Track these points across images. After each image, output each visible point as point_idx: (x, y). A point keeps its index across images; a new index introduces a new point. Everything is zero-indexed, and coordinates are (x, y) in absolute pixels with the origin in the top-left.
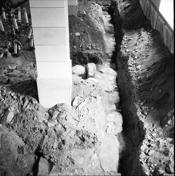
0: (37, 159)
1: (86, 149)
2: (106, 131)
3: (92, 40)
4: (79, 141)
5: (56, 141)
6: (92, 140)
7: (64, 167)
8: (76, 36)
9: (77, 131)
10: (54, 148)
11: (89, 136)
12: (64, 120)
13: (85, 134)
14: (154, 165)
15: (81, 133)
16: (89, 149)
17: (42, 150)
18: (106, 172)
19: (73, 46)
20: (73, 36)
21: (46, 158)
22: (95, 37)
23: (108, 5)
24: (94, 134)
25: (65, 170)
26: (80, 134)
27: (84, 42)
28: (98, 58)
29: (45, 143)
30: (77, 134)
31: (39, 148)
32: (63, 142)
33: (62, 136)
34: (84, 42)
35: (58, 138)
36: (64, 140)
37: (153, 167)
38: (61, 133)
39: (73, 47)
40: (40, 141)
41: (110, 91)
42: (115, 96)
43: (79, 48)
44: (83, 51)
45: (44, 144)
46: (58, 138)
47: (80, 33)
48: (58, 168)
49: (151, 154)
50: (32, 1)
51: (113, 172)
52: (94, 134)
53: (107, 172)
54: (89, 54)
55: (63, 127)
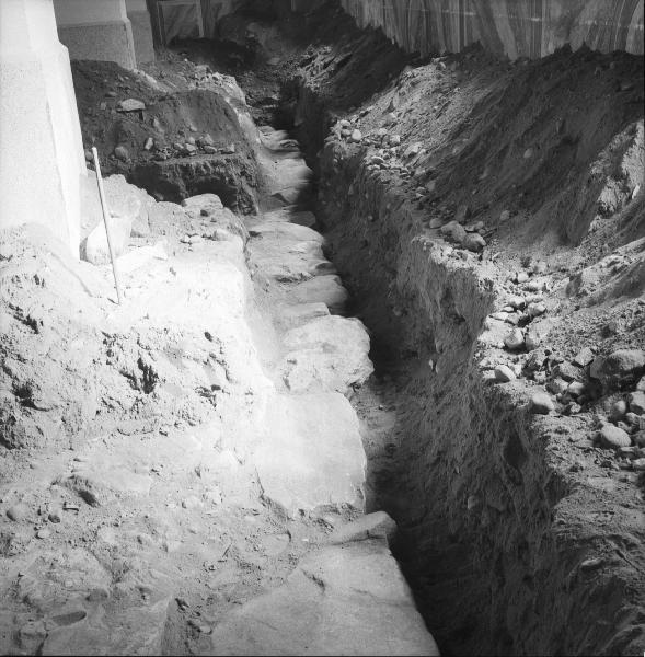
2: (286, 382)
3: (196, 123)
4: (125, 393)
6: (201, 376)
8: (124, 112)
9: (108, 340)
11: (175, 355)
13: (152, 346)
14: (577, 359)
15: (130, 345)
16: (189, 429)
18: (295, 514)
19: (116, 146)
20: (113, 111)
22: (210, 112)
23: (269, 101)
24: (208, 336)
25: (35, 540)
26: (127, 352)
27: (161, 130)
28: (231, 180)
30: (109, 353)
33: (11, 363)
34: (161, 130)
37: (573, 372)
39: (114, 153)
41: (298, 277)
42: (329, 285)
43: (144, 153)
44: (163, 160)
47: (143, 101)
49: (543, 336)
50: (151, 653)
51: (336, 511)
52: (208, 336)
53: (302, 512)
54: (186, 169)
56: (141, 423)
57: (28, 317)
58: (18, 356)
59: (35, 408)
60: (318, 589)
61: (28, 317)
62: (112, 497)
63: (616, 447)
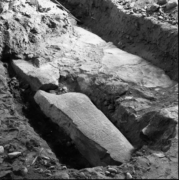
0: (8, 66)
1: (60, 35)
5: (25, 32)
7: (51, 56)
10: (26, 42)
11: (58, 19)
12: (21, 7)
16: (64, 34)
17: (12, 50)
21: (21, 59)
29: (12, 38)
31: (6, 48)
32: (34, 31)
33: (29, 24)
35: (26, 28)
36: (34, 28)
38: (26, 20)
40: (5, 38)
45: (11, 39)
46: (26, 28)
48: (44, 59)
49: (133, 6)
55: (25, 15)
56: (55, 34)
57: (25, 14)
58: (31, 22)
59: (38, 33)
60: (111, 55)
61: (25, 14)
62: (63, 48)
63: (162, 19)
